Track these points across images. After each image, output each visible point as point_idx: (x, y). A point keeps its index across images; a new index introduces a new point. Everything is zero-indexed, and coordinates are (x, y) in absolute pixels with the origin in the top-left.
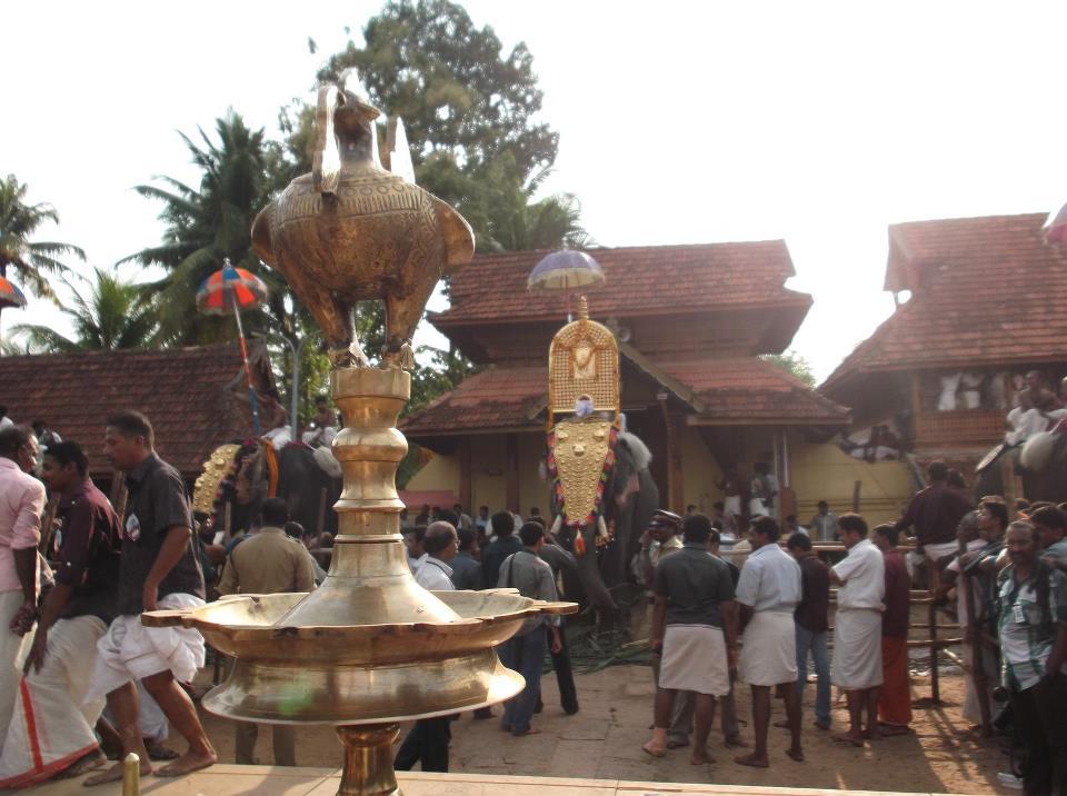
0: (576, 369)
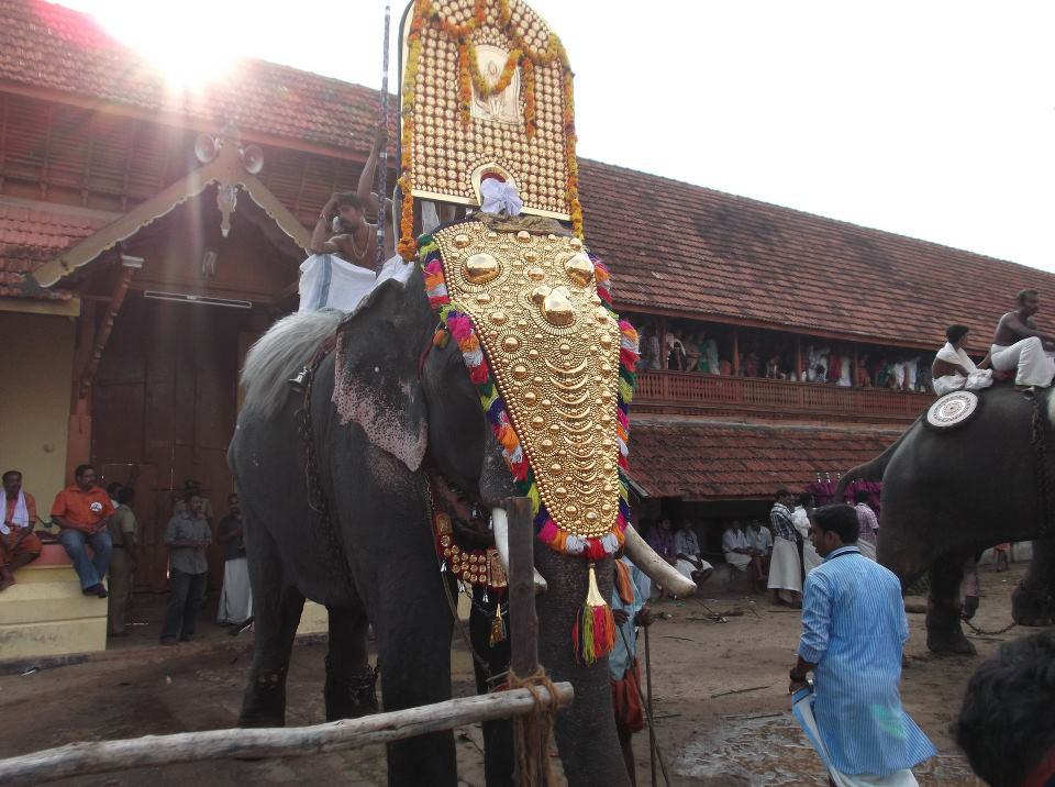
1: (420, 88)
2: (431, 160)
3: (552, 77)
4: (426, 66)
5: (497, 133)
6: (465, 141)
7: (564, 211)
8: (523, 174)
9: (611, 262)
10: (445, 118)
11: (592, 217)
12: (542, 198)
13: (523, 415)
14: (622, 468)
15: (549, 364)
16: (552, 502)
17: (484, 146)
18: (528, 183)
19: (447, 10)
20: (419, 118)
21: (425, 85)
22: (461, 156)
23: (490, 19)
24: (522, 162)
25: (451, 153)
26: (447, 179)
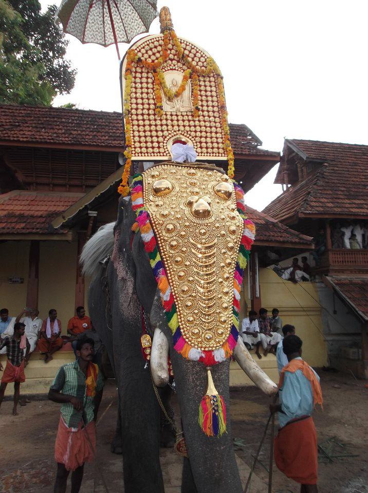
0: (164, 99)
1: (134, 101)
2: (143, 139)
3: (210, 82)
4: (136, 88)
5: (180, 118)
6: (162, 125)
7: (223, 155)
8: (197, 138)
9: (348, 194)
10: (149, 115)
12: (210, 150)
13: (174, 271)
14: (235, 307)
15: (192, 241)
16: (184, 326)
17: (173, 126)
18: (201, 142)
19: (146, 56)
20: (134, 117)
21: (136, 98)
22: (160, 134)
23: (171, 56)
24: (196, 132)
25: (154, 133)
26: (153, 148)
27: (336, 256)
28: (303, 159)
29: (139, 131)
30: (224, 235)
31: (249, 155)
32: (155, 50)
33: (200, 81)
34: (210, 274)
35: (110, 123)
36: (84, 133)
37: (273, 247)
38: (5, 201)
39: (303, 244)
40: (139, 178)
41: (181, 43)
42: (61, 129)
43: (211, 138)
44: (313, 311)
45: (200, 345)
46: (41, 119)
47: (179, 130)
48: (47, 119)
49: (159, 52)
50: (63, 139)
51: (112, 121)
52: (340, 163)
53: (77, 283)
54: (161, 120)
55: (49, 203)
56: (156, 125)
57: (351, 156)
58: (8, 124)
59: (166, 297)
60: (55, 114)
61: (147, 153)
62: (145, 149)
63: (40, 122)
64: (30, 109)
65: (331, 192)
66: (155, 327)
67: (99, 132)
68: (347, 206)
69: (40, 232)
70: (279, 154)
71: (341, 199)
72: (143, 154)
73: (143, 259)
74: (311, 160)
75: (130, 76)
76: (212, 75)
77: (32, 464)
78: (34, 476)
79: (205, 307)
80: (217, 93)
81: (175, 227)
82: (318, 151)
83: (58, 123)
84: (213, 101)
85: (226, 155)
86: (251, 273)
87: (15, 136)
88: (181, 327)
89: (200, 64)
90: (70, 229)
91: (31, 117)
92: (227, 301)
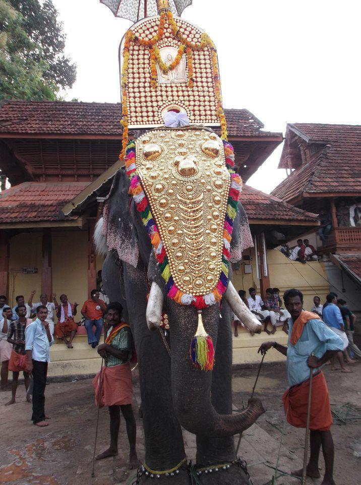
0: (159, 72)
1: (131, 75)
6: (156, 96)
7: (216, 121)
8: (190, 107)
11: (342, 152)
13: (164, 227)
15: (179, 198)
17: (167, 96)
18: (194, 111)
21: (133, 73)
22: (155, 104)
23: (167, 34)
25: (149, 104)
27: (343, 234)
28: (306, 142)
29: (135, 102)
30: (210, 189)
31: (252, 137)
32: (152, 30)
33: (194, 55)
34: (197, 227)
35: (114, 113)
36: (89, 123)
37: (279, 226)
38: (16, 192)
39: (309, 221)
40: (132, 145)
41: (177, 22)
42: (67, 121)
43: (205, 106)
44: (323, 290)
45: (191, 291)
46: (47, 112)
47: (173, 100)
48: (54, 112)
49: (155, 31)
50: (69, 130)
51: (116, 111)
52: (343, 144)
53: (89, 269)
54: (156, 91)
55: (59, 193)
56: (151, 96)
57: (353, 136)
58: (16, 118)
59: (158, 251)
60: (61, 107)
61: (142, 121)
62: (141, 118)
63: (46, 115)
64: (36, 104)
65: (334, 172)
66: (151, 281)
67: (104, 122)
68: (351, 185)
69: (52, 220)
70: (281, 134)
71: (346, 178)
72: (138, 123)
73: (137, 221)
74: (314, 142)
75: (127, 53)
76: (206, 49)
77: (53, 434)
78: (54, 444)
79: (196, 256)
80: (211, 65)
81: (162, 185)
82: (321, 133)
83: (64, 115)
84: (206, 73)
85: (219, 121)
86: (258, 252)
87: (23, 129)
88: (173, 276)
89: (195, 40)
90: (80, 216)
91: (38, 111)
92: (214, 251)
